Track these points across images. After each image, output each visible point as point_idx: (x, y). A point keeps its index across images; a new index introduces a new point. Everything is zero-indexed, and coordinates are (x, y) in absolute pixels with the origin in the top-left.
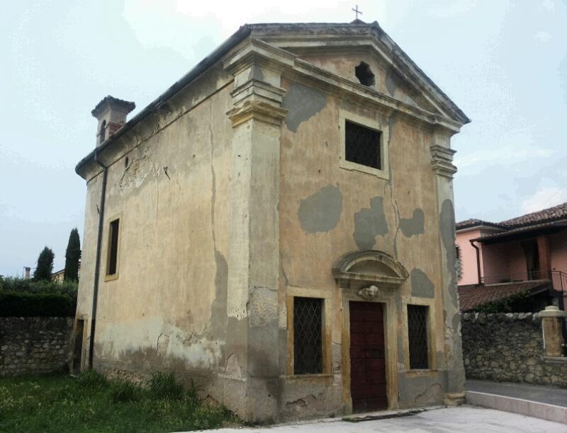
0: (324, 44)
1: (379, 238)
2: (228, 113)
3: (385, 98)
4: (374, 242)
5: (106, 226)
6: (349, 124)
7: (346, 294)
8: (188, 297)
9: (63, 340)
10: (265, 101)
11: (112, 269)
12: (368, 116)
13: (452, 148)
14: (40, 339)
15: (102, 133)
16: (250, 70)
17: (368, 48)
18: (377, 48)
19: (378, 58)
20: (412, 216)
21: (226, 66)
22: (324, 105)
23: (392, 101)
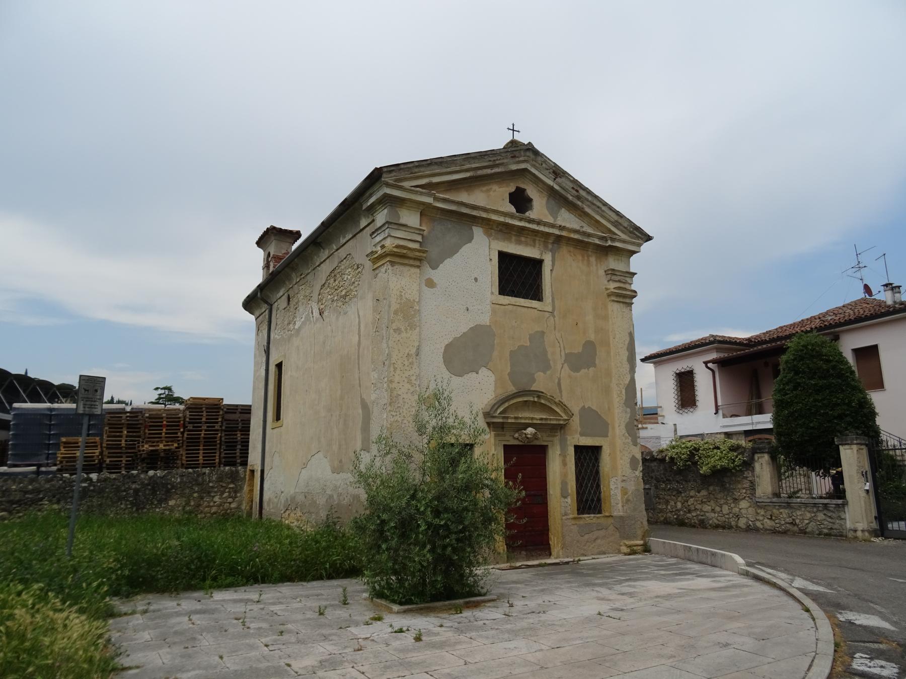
0: (467, 175)
1: (539, 376)
2: (367, 256)
3: (545, 224)
4: (534, 380)
5: (272, 368)
6: (502, 255)
7: (500, 438)
8: (340, 445)
9: (236, 492)
10: (402, 243)
11: (278, 417)
12: (527, 244)
13: (632, 270)
14: (209, 492)
15: (267, 266)
16: (386, 211)
17: (523, 173)
18: (533, 170)
19: (536, 180)
20: (580, 350)
21: (364, 207)
22: (470, 239)
23: (553, 226)
